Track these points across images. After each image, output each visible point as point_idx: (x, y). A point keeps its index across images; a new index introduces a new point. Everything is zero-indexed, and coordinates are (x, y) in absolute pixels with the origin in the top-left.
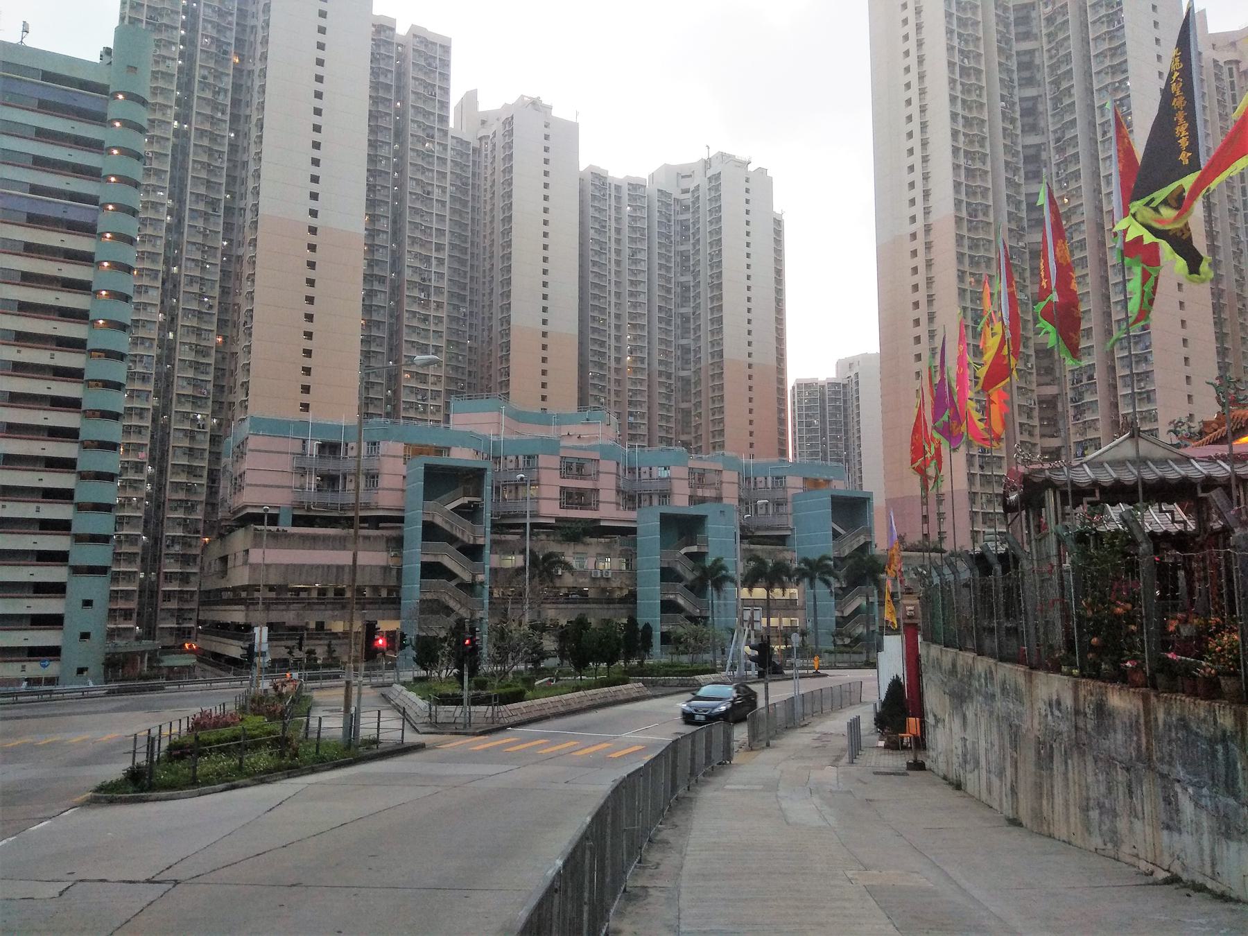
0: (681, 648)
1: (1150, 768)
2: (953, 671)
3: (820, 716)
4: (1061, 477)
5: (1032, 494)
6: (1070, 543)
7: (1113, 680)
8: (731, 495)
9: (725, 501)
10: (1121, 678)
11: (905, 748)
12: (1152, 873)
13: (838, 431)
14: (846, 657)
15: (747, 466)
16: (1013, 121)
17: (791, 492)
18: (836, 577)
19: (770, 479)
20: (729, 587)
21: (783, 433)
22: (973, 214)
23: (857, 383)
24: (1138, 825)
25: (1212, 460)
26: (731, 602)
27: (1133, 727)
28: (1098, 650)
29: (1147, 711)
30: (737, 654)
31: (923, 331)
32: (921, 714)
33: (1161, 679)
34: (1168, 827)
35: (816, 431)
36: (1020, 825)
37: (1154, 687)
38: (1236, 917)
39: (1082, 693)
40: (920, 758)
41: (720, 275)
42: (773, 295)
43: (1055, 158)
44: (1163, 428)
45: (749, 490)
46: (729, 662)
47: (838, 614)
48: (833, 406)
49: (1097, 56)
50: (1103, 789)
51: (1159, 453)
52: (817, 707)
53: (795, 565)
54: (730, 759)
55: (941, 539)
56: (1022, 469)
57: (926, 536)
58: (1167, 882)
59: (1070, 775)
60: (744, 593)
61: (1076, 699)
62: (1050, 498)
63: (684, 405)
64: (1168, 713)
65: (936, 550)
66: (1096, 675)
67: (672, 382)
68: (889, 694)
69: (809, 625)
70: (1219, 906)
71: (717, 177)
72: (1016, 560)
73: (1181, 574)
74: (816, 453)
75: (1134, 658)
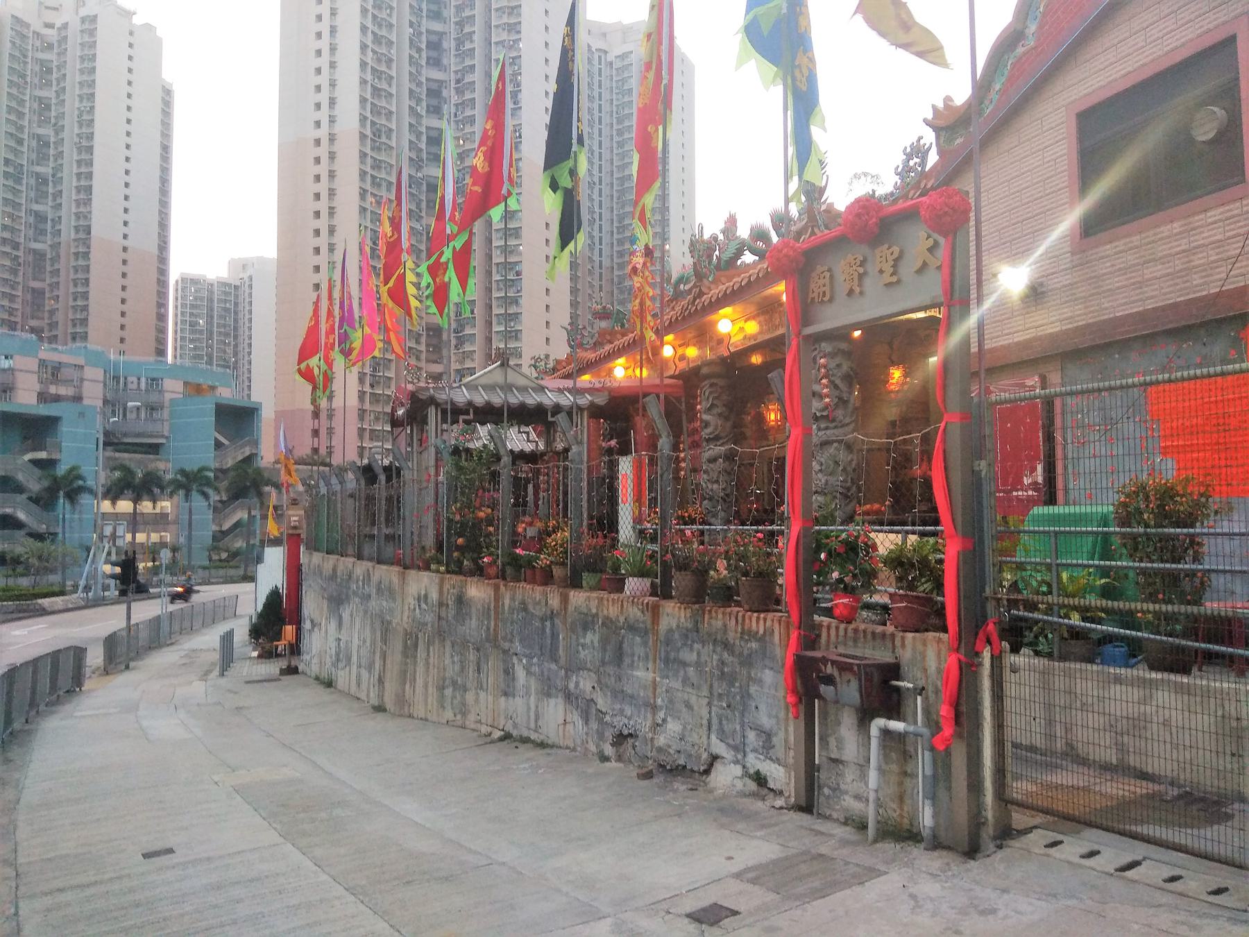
0: (20, 569)
1: (496, 646)
2: (333, 576)
3: (188, 633)
4: (442, 397)
5: (416, 412)
6: (446, 456)
7: (471, 574)
8: (93, 395)
9: (86, 402)
10: (479, 571)
11: (278, 656)
12: (490, 734)
13: (227, 335)
14: (221, 572)
15: (116, 365)
16: (419, 50)
17: (168, 396)
18: (216, 489)
19: (143, 380)
20: (85, 499)
21: (162, 331)
22: (377, 133)
23: (251, 287)
24: (482, 695)
25: (560, 391)
26: (88, 516)
27: (486, 612)
28: (463, 549)
29: (497, 599)
30: (93, 575)
31: (323, 242)
32: (297, 621)
33: (509, 570)
34: (506, 694)
35: (201, 332)
36: (385, 710)
37: (504, 578)
38: (551, 758)
39: (446, 586)
40: (293, 664)
41: (90, 137)
42: (158, 173)
43: (455, 99)
44: (526, 362)
45: (117, 390)
46: (82, 583)
47: (215, 528)
48: (221, 314)
49: (497, 10)
50: (457, 667)
51: (522, 382)
52: (187, 624)
53: (169, 476)
54: (80, 685)
55: (330, 454)
56: (410, 387)
57: (316, 450)
58: (502, 739)
59: (431, 660)
60: (106, 506)
61: (441, 592)
62: (432, 412)
63: (36, 285)
64: (513, 599)
65: (325, 465)
66: (460, 571)
67: (20, 253)
68: (267, 605)
69: (182, 540)
70: (540, 752)
71: (93, 19)
72: (398, 470)
73: (530, 487)
74: (200, 357)
75: (491, 554)
